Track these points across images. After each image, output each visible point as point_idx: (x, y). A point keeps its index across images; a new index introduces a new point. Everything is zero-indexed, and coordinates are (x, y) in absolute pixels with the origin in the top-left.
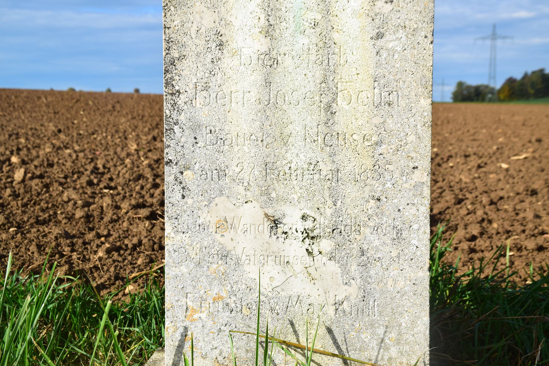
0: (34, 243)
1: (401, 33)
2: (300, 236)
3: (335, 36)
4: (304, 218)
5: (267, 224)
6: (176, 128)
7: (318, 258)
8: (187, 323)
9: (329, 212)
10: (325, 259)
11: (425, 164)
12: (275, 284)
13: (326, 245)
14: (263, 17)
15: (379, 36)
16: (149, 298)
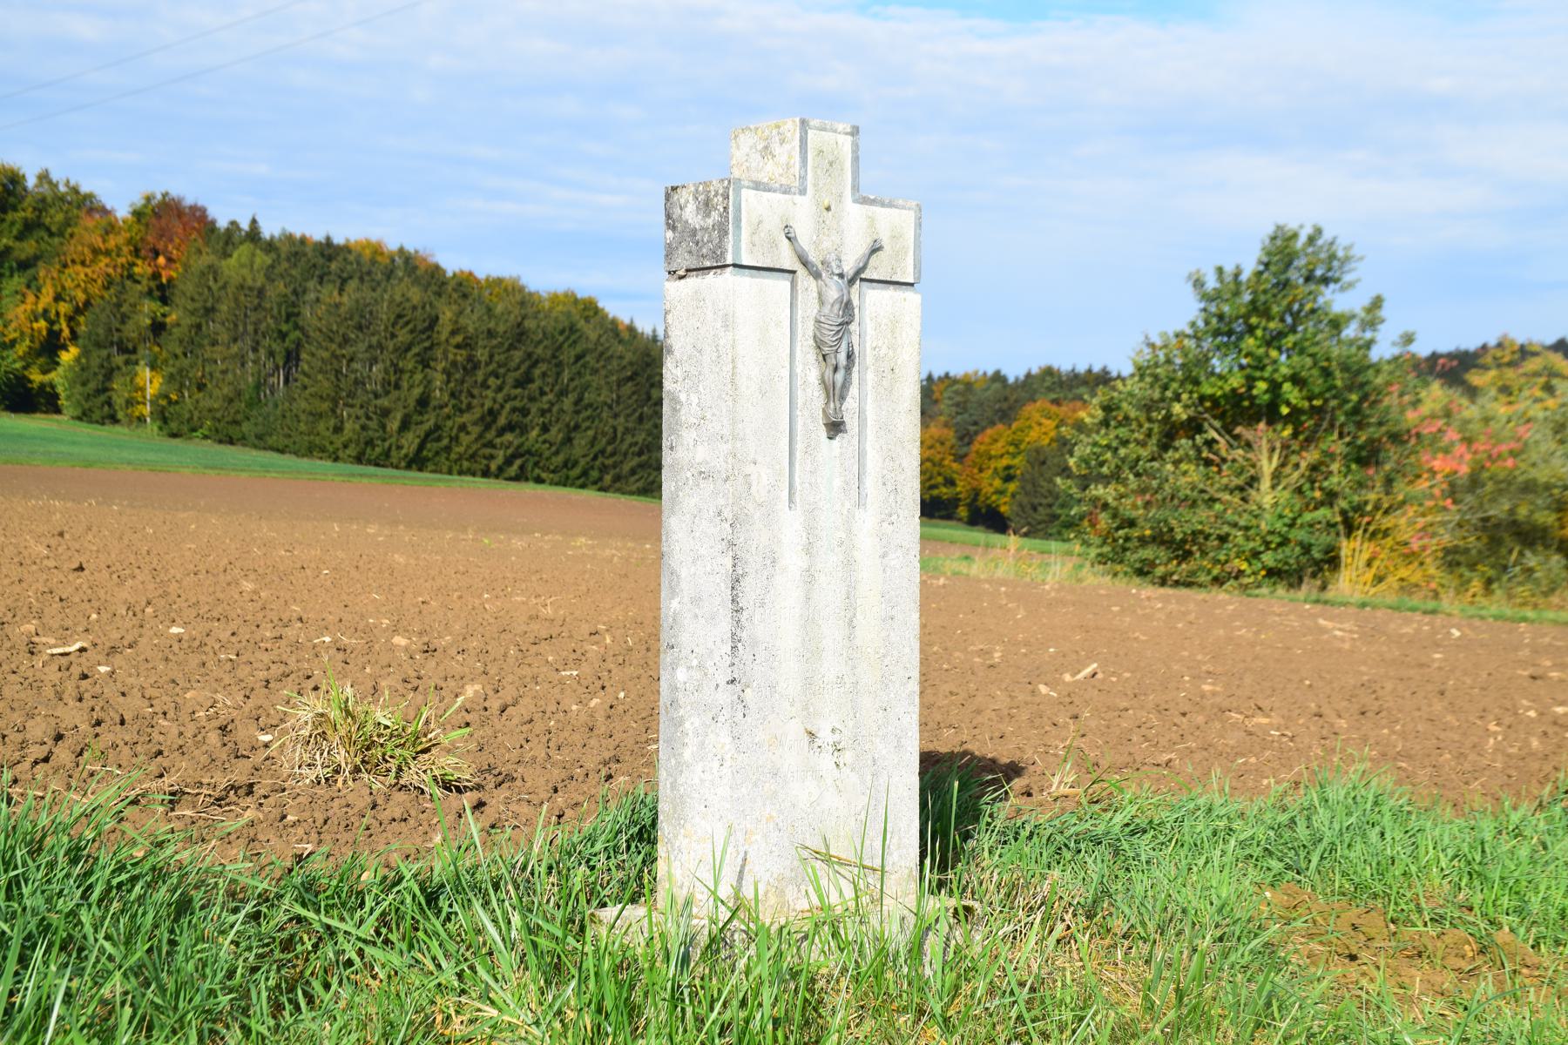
0: (597, 913)
1: (899, 553)
2: (831, 749)
3: (856, 554)
4: (833, 730)
5: (807, 738)
6: (739, 645)
7: (843, 769)
8: (746, 847)
9: (851, 724)
10: (848, 771)
11: (916, 674)
12: (813, 799)
13: (847, 757)
14: (804, 535)
15: (884, 556)
16: (510, 313)
